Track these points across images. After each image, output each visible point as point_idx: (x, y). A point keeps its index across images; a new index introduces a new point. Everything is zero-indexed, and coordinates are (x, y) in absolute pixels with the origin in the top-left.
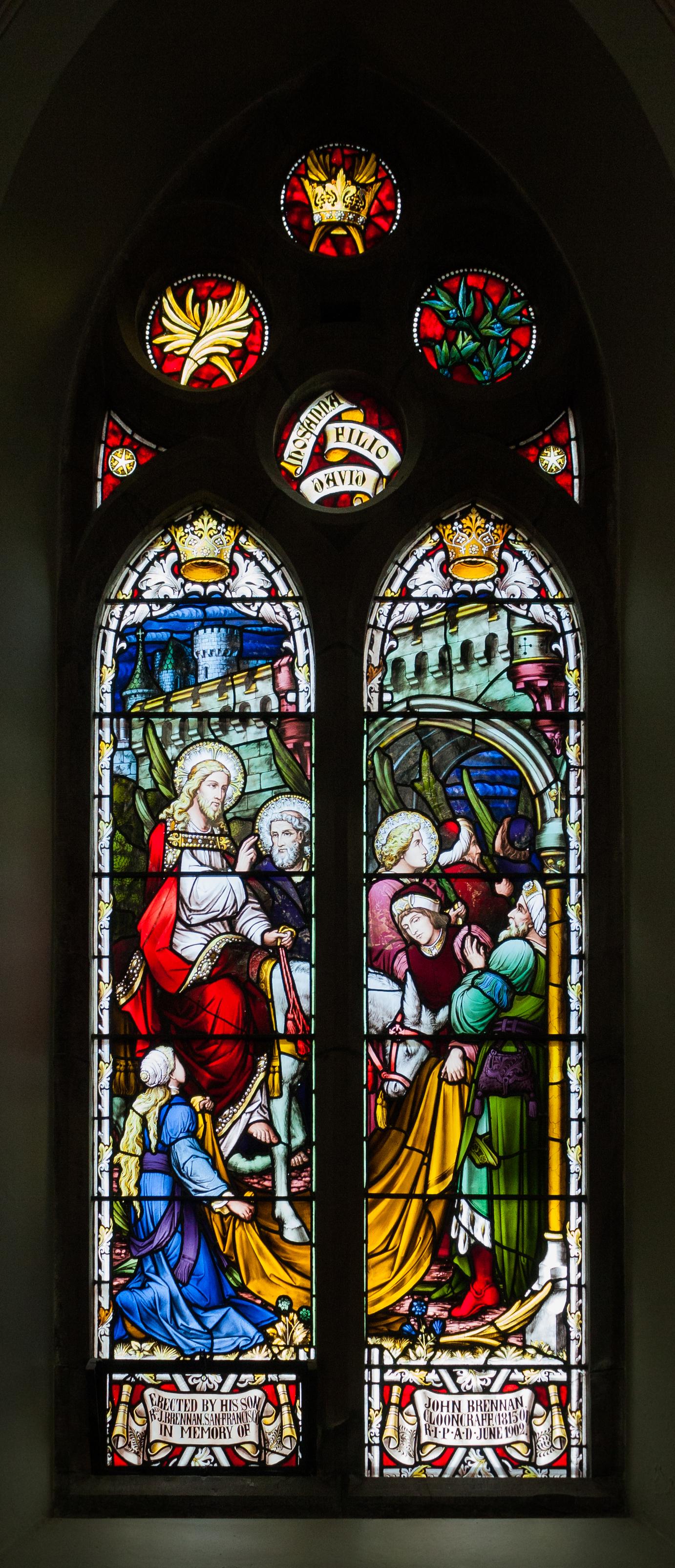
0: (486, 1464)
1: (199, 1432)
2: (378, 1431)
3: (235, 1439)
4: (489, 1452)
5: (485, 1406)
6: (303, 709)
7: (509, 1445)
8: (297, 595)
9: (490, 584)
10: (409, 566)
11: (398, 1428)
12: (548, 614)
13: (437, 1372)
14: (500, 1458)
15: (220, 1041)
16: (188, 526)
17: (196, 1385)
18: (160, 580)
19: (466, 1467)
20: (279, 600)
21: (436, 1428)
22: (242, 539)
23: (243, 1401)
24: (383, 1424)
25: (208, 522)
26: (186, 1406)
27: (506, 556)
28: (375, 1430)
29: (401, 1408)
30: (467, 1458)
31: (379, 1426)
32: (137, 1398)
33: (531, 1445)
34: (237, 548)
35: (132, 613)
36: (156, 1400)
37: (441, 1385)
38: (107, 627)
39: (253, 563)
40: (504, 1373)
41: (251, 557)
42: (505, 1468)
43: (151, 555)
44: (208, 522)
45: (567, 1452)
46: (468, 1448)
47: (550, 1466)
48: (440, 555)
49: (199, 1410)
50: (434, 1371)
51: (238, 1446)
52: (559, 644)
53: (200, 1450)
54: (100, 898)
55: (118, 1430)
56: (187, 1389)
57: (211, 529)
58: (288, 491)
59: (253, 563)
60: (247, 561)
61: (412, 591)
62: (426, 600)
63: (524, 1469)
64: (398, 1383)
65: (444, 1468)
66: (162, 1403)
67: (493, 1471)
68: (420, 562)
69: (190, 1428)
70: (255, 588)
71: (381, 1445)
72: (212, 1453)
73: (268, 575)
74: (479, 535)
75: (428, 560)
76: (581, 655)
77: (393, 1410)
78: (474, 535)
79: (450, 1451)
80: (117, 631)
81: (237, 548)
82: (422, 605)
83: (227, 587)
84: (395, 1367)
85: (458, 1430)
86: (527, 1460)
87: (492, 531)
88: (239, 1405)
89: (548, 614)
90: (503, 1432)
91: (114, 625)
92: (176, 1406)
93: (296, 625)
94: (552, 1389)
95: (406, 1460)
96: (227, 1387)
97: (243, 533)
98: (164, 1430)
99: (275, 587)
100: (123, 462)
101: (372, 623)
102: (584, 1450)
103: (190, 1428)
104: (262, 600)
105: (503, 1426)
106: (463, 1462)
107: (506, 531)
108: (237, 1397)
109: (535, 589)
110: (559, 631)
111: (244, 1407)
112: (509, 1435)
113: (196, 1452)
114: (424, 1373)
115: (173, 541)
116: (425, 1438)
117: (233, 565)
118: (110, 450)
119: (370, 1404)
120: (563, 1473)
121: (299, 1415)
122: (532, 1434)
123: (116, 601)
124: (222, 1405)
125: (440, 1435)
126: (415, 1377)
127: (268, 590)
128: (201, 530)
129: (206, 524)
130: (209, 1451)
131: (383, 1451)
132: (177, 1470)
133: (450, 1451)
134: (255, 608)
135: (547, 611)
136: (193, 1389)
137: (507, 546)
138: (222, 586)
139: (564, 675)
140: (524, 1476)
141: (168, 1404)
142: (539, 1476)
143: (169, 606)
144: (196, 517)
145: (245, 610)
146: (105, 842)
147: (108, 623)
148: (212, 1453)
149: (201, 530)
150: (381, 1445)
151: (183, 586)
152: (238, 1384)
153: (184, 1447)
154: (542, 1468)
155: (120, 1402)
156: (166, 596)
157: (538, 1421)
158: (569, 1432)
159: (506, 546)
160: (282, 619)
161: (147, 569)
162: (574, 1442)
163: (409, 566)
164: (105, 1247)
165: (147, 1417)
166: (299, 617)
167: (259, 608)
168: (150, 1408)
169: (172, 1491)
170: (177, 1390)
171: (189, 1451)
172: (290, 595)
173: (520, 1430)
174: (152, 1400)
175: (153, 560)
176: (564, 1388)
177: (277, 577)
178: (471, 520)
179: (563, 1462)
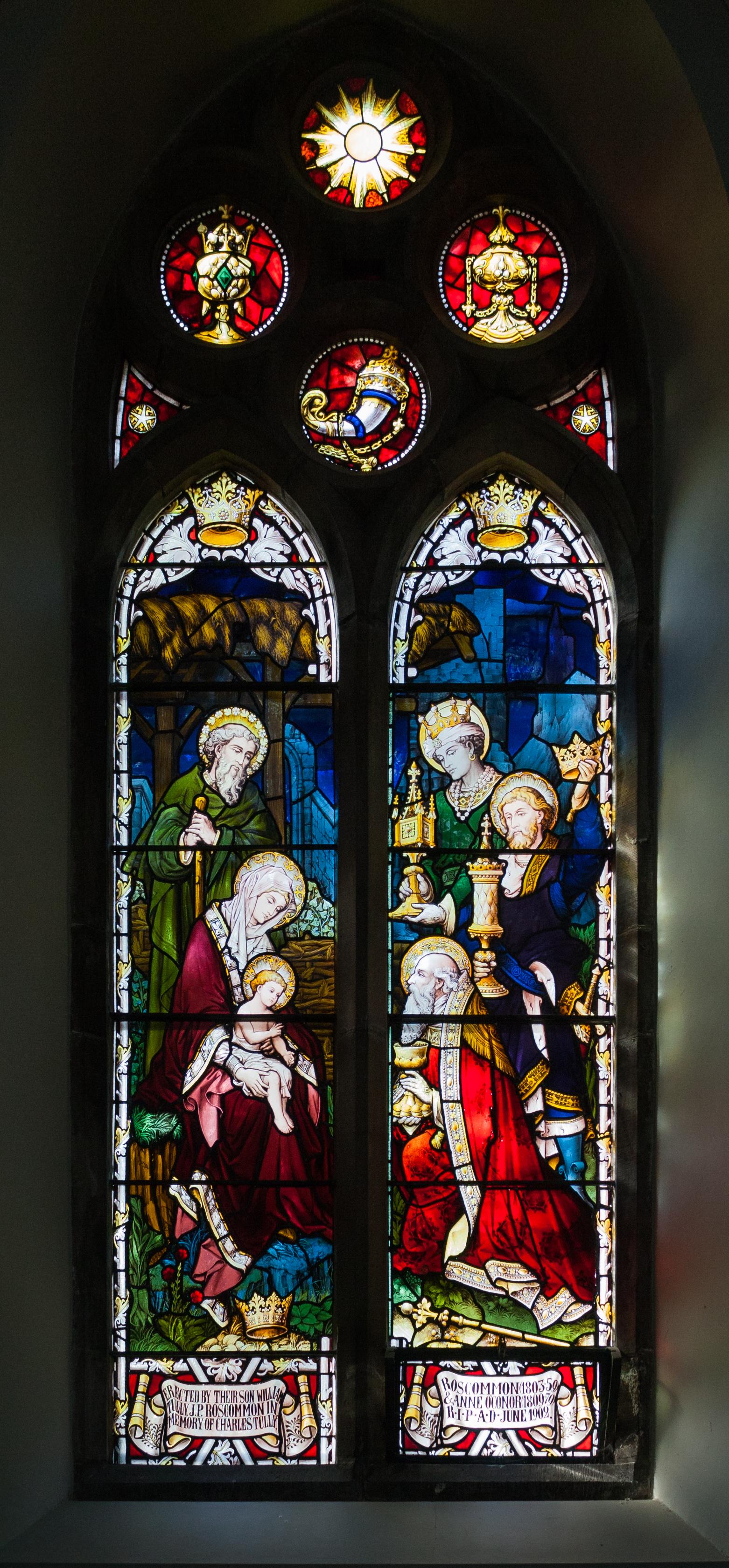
0: (509, 1447)
2: (123, 1422)
4: (512, 1435)
10: (156, 534)
12: (299, 580)
13: (185, 1361)
14: (522, 1440)
15: (186, 1023)
16: (484, 491)
17: (215, 1375)
18: (455, 548)
19: (490, 1451)
20: (300, 565)
22: (542, 505)
24: (129, 1415)
25: (227, 484)
27: (537, 524)
28: (121, 1421)
31: (125, 1417)
32: (430, 1381)
33: (556, 1429)
34: (536, 514)
35: (147, 579)
38: (401, 599)
39: (273, 528)
40: (255, 1361)
41: (548, 523)
42: (529, 1450)
43: (168, 519)
44: (227, 484)
45: (316, 1442)
46: (492, 1430)
47: (300, 1457)
48: (468, 525)
52: (589, 613)
53: (220, 1442)
55: (411, 1412)
57: (507, 494)
60: (267, 526)
61: (439, 560)
62: (452, 568)
65: (467, 1450)
68: (446, 531)
71: (127, 1436)
72: (232, 1446)
73: (569, 544)
74: (507, 502)
75: (454, 529)
77: (140, 1398)
79: (474, 1433)
81: (536, 514)
82: (448, 573)
84: (142, 1356)
86: (551, 1443)
87: (520, 498)
89: (299, 580)
90: (527, 1415)
91: (127, 592)
93: (598, 596)
94: (302, 1379)
95: (150, 1450)
100: (144, 418)
101: (398, 596)
102: (334, 1440)
104: (282, 566)
105: (528, 1409)
106: (485, 1446)
107: (535, 497)
109: (286, 556)
110: (589, 600)
112: (533, 1417)
113: (216, 1445)
116: (448, 1421)
118: (130, 408)
121: (596, 1404)
122: (557, 1416)
123: (412, 569)
125: (464, 1417)
126: (163, 1365)
129: (224, 486)
130: (229, 1444)
131: (130, 1443)
133: (474, 1433)
134: (555, 576)
135: (297, 577)
136: (212, 1380)
138: (520, 555)
139: (595, 646)
144: (215, 479)
147: (402, 595)
148: (232, 1446)
149: (218, 492)
150: (127, 1436)
151: (480, 554)
152: (258, 1374)
153: (204, 1439)
154: (292, 1458)
155: (137, 1392)
159: (536, 514)
160: (303, 588)
162: (324, 1432)
163: (156, 534)
166: (600, 586)
167: (280, 573)
170: (196, 1382)
171: (209, 1444)
173: (544, 1414)
176: (313, 1378)
177: (577, 545)
178: (499, 486)
179: (313, 1451)
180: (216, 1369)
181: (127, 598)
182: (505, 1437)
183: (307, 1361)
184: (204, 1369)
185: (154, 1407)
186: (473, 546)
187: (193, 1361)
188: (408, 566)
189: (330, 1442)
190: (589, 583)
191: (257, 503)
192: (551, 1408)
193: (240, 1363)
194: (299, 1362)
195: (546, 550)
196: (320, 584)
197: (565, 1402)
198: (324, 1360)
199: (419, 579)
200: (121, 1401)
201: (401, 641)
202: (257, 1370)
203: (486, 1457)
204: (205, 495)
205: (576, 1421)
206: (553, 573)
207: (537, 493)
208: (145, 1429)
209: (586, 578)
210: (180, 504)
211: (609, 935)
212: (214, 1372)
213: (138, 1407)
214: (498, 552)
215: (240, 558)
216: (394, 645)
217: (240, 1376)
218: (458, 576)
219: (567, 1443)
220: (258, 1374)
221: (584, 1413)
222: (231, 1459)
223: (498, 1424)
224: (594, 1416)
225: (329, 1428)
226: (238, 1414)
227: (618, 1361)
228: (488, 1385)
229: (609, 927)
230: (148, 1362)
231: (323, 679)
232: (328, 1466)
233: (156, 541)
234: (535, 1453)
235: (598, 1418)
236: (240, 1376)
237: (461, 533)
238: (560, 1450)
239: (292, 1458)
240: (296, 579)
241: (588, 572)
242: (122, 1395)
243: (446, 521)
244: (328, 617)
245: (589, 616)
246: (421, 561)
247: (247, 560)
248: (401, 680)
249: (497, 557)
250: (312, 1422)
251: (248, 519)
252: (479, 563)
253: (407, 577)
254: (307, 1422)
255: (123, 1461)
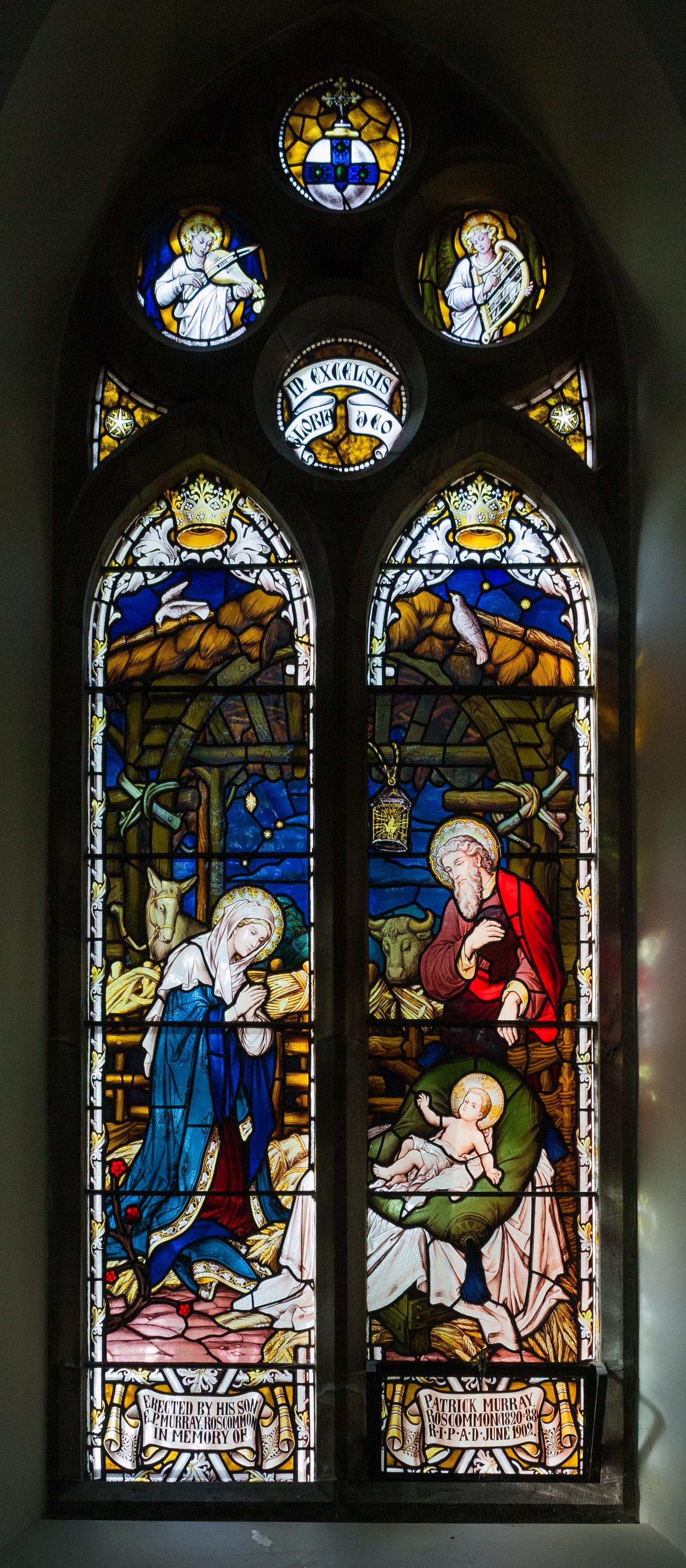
1: (190, 1436)
3: (231, 1445)
4: (498, 1453)
5: (160, 1406)
6: (301, 682)
7: (519, 1446)
8: (575, 561)
9: (218, 552)
11: (120, 1432)
12: (278, 581)
13: (161, 1371)
18: (154, 547)
19: (476, 1470)
21: (441, 1429)
23: (240, 1404)
26: (181, 1408)
29: (123, 1410)
30: (476, 1461)
31: (101, 1426)
33: (540, 1446)
35: (126, 581)
36: (150, 1402)
37: (444, 1383)
38: (99, 599)
40: (231, 1372)
41: (252, 523)
44: (483, 486)
45: (295, 1455)
46: (477, 1449)
47: (276, 1470)
49: (195, 1413)
50: (157, 1370)
51: (235, 1451)
52: (287, 610)
53: (196, 1455)
54: (93, 879)
55: (393, 1432)
56: (181, 1391)
58: (287, 456)
59: (530, 530)
62: (430, 566)
63: (250, 1474)
64: (122, 1382)
65: (169, 1473)
66: (156, 1404)
67: (218, 1477)
68: (425, 530)
69: (181, 1432)
70: (254, 554)
71: (102, 1447)
72: (208, 1459)
73: (267, 540)
75: (432, 528)
76: (92, 624)
77: (115, 1411)
78: (480, 502)
80: (388, 601)
83: (224, 554)
84: (117, 1366)
85: (464, 1430)
86: (537, 1461)
88: (236, 1408)
89: (278, 581)
90: (510, 1433)
92: (170, 1407)
93: (296, 593)
96: (501, 1387)
97: (243, 495)
98: (160, 1434)
99: (552, 554)
101: (96, 596)
102: (312, 1453)
103: (201, 1433)
104: (261, 567)
106: (471, 1464)
108: (236, 1399)
110: (289, 599)
111: (241, 1411)
112: (517, 1435)
113: (192, 1458)
114: (146, 1372)
115: (447, 507)
116: (430, 1440)
117: (229, 529)
119: (92, 1403)
120: (289, 1477)
121: (581, 1419)
122: (541, 1433)
124: (218, 1408)
127: (267, 556)
128: (196, 493)
129: (480, 489)
131: (104, 1454)
132: (453, 1476)
136: (187, 1391)
137: (513, 514)
140: (251, 1480)
141: (163, 1407)
142: (266, 1480)
143: (165, 575)
144: (470, 481)
145: (243, 577)
146: (98, 821)
147: (100, 594)
148: (208, 1459)
149: (474, 494)
151: (179, 554)
152: (234, 1386)
154: (269, 1471)
156: (161, 563)
157: (266, 1422)
158: (296, 1433)
161: (142, 534)
162: (301, 1444)
163: (134, 536)
164: (98, 1243)
165: (141, 1419)
167: (258, 575)
168: (143, 1408)
169: (453, 1498)
170: (173, 1393)
172: (569, 561)
173: (528, 1430)
174: (146, 1402)
175: (149, 526)
178: (477, 487)
179: (290, 1466)
180: (192, 1379)
181: (384, 600)
182: (492, 1455)
183: (283, 1372)
184: (180, 1379)
185: (411, 1417)
186: (173, 546)
187: (168, 1371)
188: (106, 565)
189: (308, 1455)
190: (567, 583)
191: (235, 503)
192: (535, 1424)
193: (216, 1373)
194: (274, 1373)
195: (526, 548)
196: (299, 584)
197: (548, 1419)
198: (300, 1372)
199: (397, 576)
200: (97, 1410)
201: (378, 640)
202: (234, 1381)
203: (473, 1474)
204: (461, 499)
205: (560, 1438)
206: (531, 573)
207: (236, 492)
208: (121, 1446)
209: (564, 578)
210: (158, 506)
211: (591, 938)
212: (190, 1382)
213: (113, 1422)
214: (478, 552)
215: (220, 558)
216: (371, 645)
217: (216, 1387)
218: (437, 576)
219: (269, 1465)
220: (234, 1386)
221: (568, 1430)
222: (207, 1472)
223: (481, 1443)
224: (578, 1431)
225: (306, 1440)
226: (236, 1426)
227: (603, 1378)
228: (491, 1400)
229: (590, 929)
230: (123, 1372)
231: (301, 682)
232: (307, 1484)
233: (135, 544)
234: (521, 1472)
235: (582, 1433)
236: (216, 1387)
237: (161, 532)
238: (547, 1468)
239: (269, 1471)
240: (554, 583)
241: (566, 571)
242: (98, 1404)
243: (424, 520)
244: (307, 616)
245: (568, 618)
246: (120, 559)
247: (504, 562)
248: (379, 682)
249: (195, 556)
250: (290, 1436)
251: (505, 522)
252: (457, 562)
253: (105, 577)
254: (285, 1435)
255: (383, 1470)
